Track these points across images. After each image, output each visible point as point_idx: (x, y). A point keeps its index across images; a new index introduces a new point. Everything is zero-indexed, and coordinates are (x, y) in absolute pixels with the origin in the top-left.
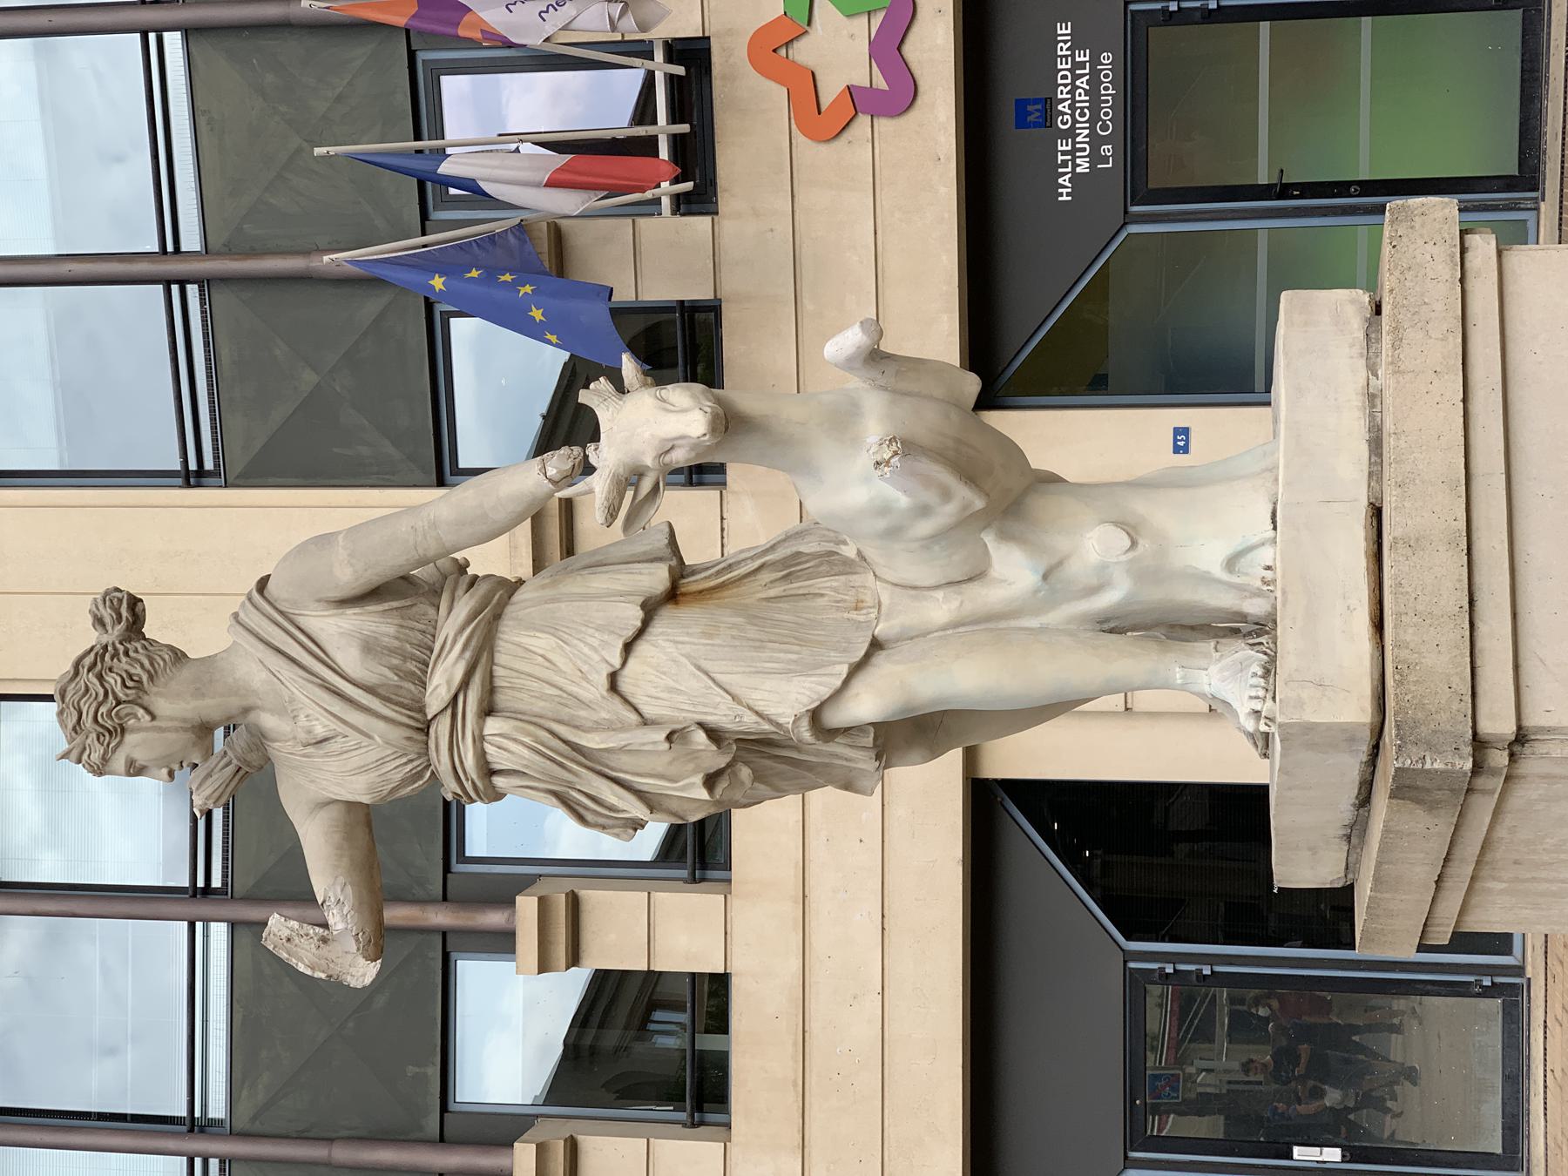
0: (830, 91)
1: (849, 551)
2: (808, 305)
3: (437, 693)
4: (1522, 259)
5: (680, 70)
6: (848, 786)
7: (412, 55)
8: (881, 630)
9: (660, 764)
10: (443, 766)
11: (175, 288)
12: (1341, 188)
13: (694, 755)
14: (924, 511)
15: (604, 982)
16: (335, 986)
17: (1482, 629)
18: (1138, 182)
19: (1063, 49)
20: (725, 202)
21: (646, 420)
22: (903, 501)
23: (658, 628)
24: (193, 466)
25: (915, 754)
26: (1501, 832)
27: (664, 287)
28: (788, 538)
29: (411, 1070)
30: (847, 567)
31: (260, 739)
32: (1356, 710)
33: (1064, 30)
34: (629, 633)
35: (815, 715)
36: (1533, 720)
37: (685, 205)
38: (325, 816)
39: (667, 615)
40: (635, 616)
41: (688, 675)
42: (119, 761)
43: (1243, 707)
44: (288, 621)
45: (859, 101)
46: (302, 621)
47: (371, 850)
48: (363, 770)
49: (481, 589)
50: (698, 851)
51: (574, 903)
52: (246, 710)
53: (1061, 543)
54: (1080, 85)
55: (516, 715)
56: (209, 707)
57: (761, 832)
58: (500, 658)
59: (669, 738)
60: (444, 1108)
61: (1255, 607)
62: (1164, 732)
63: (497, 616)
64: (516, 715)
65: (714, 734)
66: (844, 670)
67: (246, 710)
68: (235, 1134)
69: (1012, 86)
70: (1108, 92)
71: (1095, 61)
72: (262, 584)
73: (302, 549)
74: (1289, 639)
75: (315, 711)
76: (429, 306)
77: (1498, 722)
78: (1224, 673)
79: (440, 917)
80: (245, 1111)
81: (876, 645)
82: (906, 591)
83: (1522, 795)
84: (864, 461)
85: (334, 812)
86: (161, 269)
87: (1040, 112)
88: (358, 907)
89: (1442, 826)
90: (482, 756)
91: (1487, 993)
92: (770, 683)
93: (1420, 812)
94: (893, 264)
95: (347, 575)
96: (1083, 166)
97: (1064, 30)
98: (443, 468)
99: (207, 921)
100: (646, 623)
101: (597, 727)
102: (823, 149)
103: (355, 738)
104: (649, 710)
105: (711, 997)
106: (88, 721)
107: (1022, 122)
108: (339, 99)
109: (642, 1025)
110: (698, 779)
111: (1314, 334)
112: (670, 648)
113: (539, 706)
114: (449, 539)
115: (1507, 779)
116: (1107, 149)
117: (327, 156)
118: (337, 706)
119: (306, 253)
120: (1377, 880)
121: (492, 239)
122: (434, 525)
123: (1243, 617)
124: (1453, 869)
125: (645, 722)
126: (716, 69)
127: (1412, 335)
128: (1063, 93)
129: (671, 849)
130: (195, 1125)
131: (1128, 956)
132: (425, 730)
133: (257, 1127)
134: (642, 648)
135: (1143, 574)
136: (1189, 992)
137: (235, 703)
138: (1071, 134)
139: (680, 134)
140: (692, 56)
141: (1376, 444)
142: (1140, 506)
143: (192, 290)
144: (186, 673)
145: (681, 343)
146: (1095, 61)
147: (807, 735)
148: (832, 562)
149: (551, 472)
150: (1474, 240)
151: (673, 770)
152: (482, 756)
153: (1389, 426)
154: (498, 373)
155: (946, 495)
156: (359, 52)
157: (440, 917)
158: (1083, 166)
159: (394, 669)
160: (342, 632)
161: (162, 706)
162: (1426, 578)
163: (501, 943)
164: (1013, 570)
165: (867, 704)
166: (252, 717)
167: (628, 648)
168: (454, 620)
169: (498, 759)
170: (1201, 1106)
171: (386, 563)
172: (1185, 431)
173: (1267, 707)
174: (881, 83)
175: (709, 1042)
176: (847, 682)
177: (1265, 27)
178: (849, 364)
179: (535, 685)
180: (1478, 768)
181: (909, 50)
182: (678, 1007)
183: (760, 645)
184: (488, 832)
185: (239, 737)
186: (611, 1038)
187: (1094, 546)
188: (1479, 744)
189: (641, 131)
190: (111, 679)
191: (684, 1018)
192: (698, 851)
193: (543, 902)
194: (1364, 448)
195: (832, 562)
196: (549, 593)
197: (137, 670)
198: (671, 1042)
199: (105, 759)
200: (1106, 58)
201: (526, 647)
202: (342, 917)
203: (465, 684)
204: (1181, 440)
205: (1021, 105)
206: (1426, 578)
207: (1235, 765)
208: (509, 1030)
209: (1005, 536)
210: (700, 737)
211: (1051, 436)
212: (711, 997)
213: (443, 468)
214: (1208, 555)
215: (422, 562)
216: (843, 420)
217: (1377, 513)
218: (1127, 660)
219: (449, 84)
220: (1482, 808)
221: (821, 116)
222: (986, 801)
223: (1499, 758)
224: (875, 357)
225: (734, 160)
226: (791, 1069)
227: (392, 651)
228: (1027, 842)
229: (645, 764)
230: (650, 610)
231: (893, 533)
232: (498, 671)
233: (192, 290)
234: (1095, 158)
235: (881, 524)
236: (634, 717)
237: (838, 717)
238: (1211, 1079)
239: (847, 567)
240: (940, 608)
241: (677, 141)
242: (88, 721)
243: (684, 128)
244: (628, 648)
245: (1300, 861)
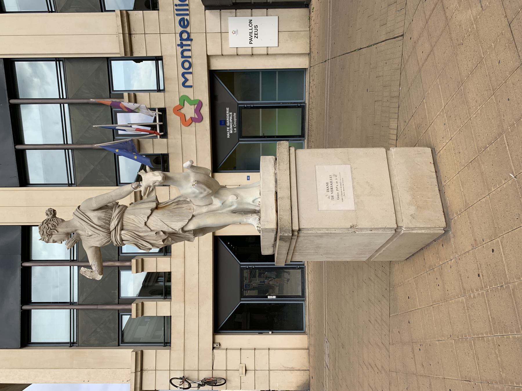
0: (188, 118)
1: (188, 200)
2: (184, 155)
3: (112, 227)
4: (299, 151)
5: (161, 113)
6: (189, 240)
7: (111, 109)
8: (194, 213)
9: (154, 238)
10: (114, 240)
11: (67, 150)
12: (273, 137)
13: (160, 236)
14: (201, 193)
15: (149, 275)
16: (94, 280)
17: (293, 212)
18: (240, 134)
19: (227, 112)
20: (169, 136)
21: (152, 177)
22: (197, 191)
23: (154, 214)
24: (70, 183)
25: (201, 235)
26: (297, 245)
27: (159, 150)
28: (177, 197)
29: (112, 291)
30: (188, 202)
31: (79, 235)
32: (274, 226)
33: (228, 109)
34: (149, 215)
35: (182, 229)
36: (301, 227)
37: (162, 137)
38: (91, 249)
39: (156, 211)
40: (150, 212)
41: (160, 222)
42: (51, 240)
43: (256, 226)
44: (84, 214)
45: (193, 120)
46: (86, 214)
47: (100, 254)
48: (98, 241)
49: (121, 207)
50: (166, 251)
51: (143, 260)
52: (76, 230)
53: (225, 198)
54: (231, 119)
55: (127, 230)
56: (69, 230)
57: (177, 248)
58: (124, 220)
59: (156, 233)
60: (119, 298)
61: (257, 209)
62: (248, 227)
63: (124, 212)
64: (127, 230)
65: (164, 232)
66: (187, 221)
67: (76, 230)
68: (79, 305)
69: (219, 118)
70: (235, 120)
71: (233, 114)
72: (79, 207)
73: (86, 201)
74: (262, 214)
75: (89, 230)
76: (115, 154)
77: (296, 228)
78: (252, 220)
79: (118, 264)
80: (81, 300)
81: (193, 216)
82: (198, 206)
83: (300, 239)
84: (190, 185)
85: (93, 248)
86: (64, 147)
87: (224, 123)
88: (98, 266)
89: (287, 244)
90: (121, 238)
91: (299, 269)
92: (174, 223)
93: (284, 242)
94: (199, 148)
95: (95, 206)
96: (231, 132)
97: (228, 109)
98: (117, 183)
99: (73, 266)
100: (152, 213)
101: (143, 232)
102: (187, 128)
103: (97, 235)
104: (152, 229)
105: (168, 276)
106: (45, 233)
107: (221, 124)
108: (98, 117)
109: (157, 282)
110: (161, 240)
111: (266, 162)
112: (156, 218)
113: (132, 228)
114: (114, 199)
115: (298, 236)
116: (235, 129)
117: (95, 127)
118: (93, 229)
119: (92, 144)
120: (278, 253)
121: (126, 142)
122: (111, 196)
123: (256, 210)
124: (290, 251)
125: (152, 231)
126: (167, 114)
127: (281, 164)
128: (228, 119)
129: (161, 251)
130: (71, 303)
131: (241, 265)
132: (110, 233)
133: (83, 303)
134: (151, 217)
135: (239, 203)
136: (252, 270)
137: (74, 229)
138: (229, 126)
139: (161, 126)
140: (163, 111)
141: (276, 182)
142: (238, 192)
143: (70, 151)
144: (64, 223)
145: (161, 162)
146: (233, 114)
147: (181, 232)
148: (185, 202)
149: (133, 187)
150: (291, 148)
151: (157, 239)
152: (121, 238)
153: (278, 179)
154: (128, 166)
155: (205, 190)
156: (102, 109)
157: (118, 264)
158: (231, 132)
159: (104, 222)
160: (94, 216)
161: (60, 230)
162: (284, 204)
163: (129, 268)
164: (217, 203)
165: (192, 226)
166: (77, 232)
167: (148, 218)
168: (115, 213)
169: (124, 238)
170: (254, 289)
171: (102, 203)
172: (249, 176)
173: (259, 225)
174: (196, 117)
175: (167, 284)
176: (188, 223)
177: (261, 110)
178: (188, 168)
179: (131, 224)
180: (293, 235)
181: (201, 111)
182: (162, 277)
183: (172, 216)
184: (126, 249)
185: (75, 235)
186: (151, 284)
187: (231, 198)
188: (293, 231)
189: (154, 124)
190: (49, 225)
191: (163, 279)
192: (166, 251)
193: (137, 260)
194: (274, 182)
195: (185, 202)
196: (134, 208)
197: (55, 223)
198: (162, 283)
199: (48, 240)
200: (235, 114)
201: (129, 218)
202: (95, 267)
203: (118, 225)
204: (248, 178)
205: (221, 121)
206: (284, 204)
207: (257, 234)
208: (131, 283)
209: (215, 197)
210: (162, 233)
211: (225, 178)
212: (168, 276)
213: (117, 183)
214: (250, 200)
215: (110, 203)
216: (187, 177)
217: (276, 193)
218: (237, 218)
219: (118, 114)
220: (294, 242)
221: (186, 122)
222: (216, 239)
223: (296, 233)
224: (192, 167)
225: (170, 130)
226: (182, 288)
227: (104, 219)
228: (224, 247)
229: (151, 238)
230: (152, 211)
231: (196, 197)
232: (124, 222)
233: (70, 151)
234: (233, 131)
235: (194, 195)
236: (149, 230)
237: (186, 229)
238: (255, 284)
239: (188, 202)
240: (204, 210)
241: (160, 126)
242: (45, 233)
243: (162, 123)
244: (148, 218)
245: (266, 251)
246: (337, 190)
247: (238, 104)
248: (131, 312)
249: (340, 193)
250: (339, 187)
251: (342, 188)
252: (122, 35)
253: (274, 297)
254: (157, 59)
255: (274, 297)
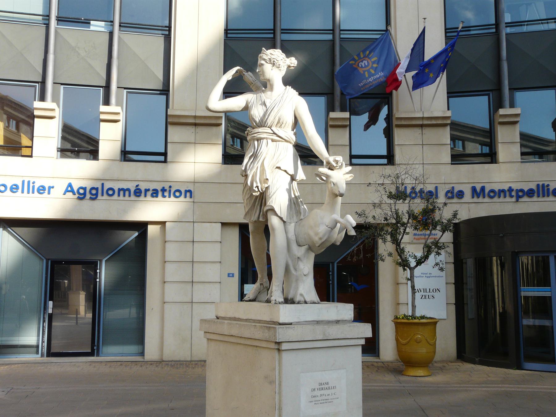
4: (360, 349)
100: (290, 175)
167: (285, 171)
172: (233, 276)
204: (231, 275)
233: (272, 36)
246: (321, 395)
247: (333, 263)
248: (40, 101)
249: (317, 399)
250: (324, 397)
251: (323, 401)
252: (421, 116)
253: (50, 311)
254: (390, 158)
255: (50, 311)
